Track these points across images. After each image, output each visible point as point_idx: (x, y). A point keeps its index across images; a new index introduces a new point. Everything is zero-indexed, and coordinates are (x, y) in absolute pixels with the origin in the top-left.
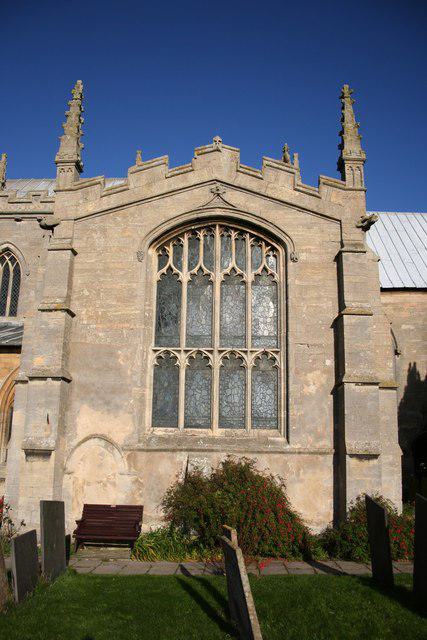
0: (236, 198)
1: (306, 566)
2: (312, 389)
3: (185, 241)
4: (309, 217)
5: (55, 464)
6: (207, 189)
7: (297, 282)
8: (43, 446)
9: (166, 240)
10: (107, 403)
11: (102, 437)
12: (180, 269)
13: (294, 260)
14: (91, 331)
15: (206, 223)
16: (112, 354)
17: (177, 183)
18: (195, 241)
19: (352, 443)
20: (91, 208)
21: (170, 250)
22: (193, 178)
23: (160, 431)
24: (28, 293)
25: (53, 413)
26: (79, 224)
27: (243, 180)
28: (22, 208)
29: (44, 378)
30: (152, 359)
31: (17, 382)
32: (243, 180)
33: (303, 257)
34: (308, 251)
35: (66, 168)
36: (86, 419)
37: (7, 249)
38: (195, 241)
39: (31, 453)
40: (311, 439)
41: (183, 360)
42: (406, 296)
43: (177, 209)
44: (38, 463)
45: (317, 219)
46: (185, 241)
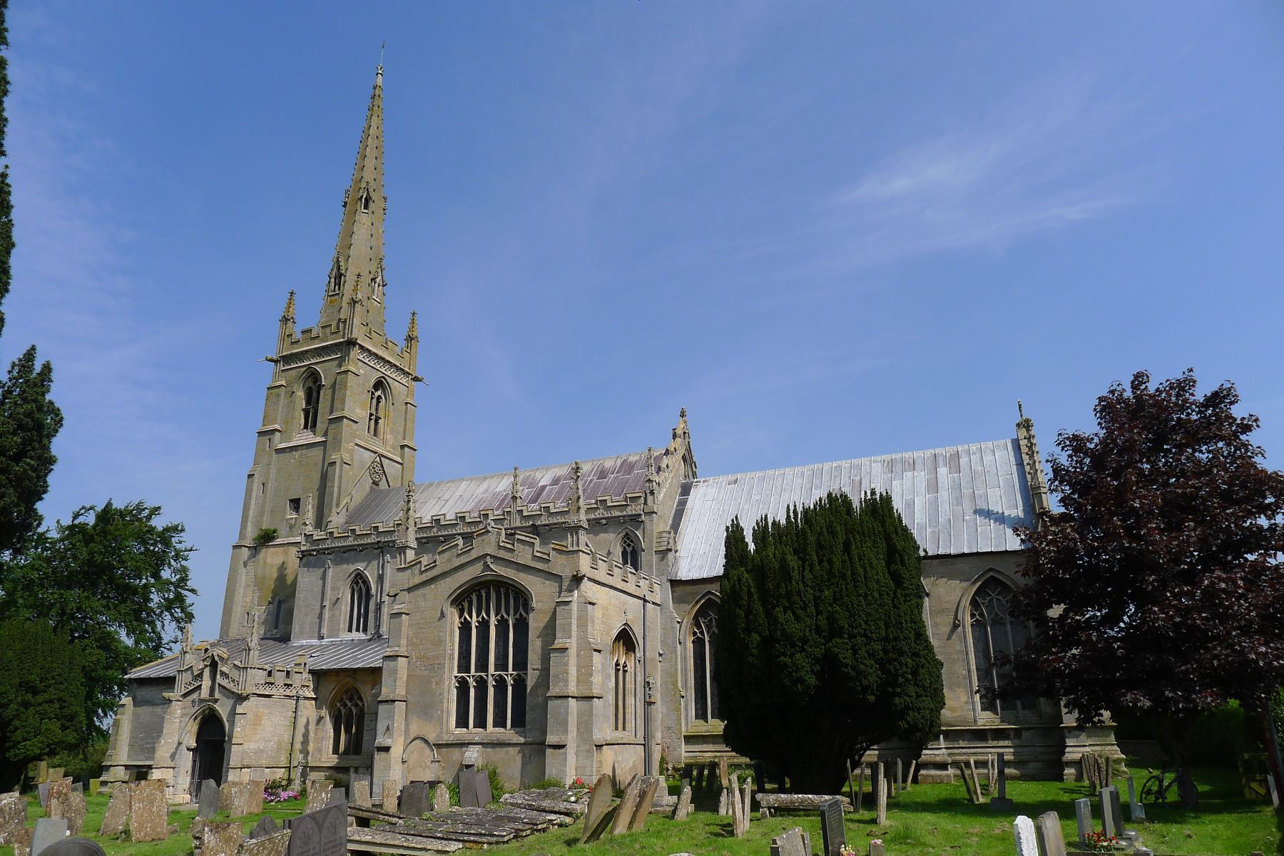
3: (474, 597)
10: (426, 714)
21: (466, 604)
37: (358, 574)
46: (474, 597)
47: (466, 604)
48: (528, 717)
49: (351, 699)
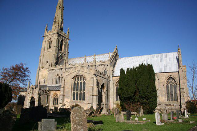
0: (81, 72)
1: (136, 95)
3: (76, 78)
4: (88, 74)
9: (74, 78)
14: (66, 90)
15: (78, 75)
16: (68, 92)
17: (75, 71)
18: (77, 78)
19: (180, 77)
20: (66, 75)
21: (75, 79)
22: (76, 70)
23: (73, 101)
25: (62, 99)
27: (81, 70)
32: (81, 70)
36: (66, 100)
39: (60, 103)
42: (174, 73)
43: (74, 74)
44: (61, 104)
46: (76, 78)
47: (75, 79)
48: (85, 99)
49: (56, 95)
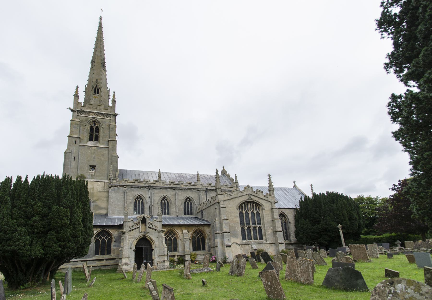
2: (270, 233)
3: (243, 205)
5: (363, 238)
6: (248, 195)
7: (265, 214)
8: (230, 245)
10: (236, 236)
11: (236, 243)
12: (243, 210)
13: (264, 210)
18: (245, 205)
20: (226, 198)
24: (173, 209)
26: (225, 202)
28: (168, 186)
29: (227, 233)
30: (240, 228)
31: (215, 234)
33: (265, 209)
34: (266, 208)
35: (219, 190)
38: (245, 205)
40: (270, 241)
41: (246, 228)
45: (267, 202)
